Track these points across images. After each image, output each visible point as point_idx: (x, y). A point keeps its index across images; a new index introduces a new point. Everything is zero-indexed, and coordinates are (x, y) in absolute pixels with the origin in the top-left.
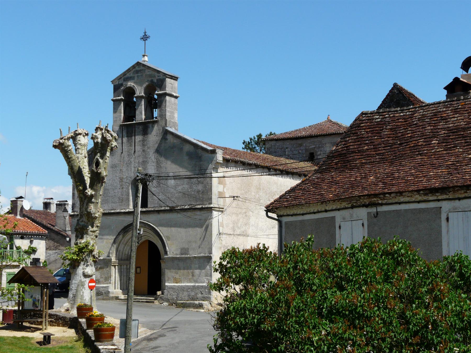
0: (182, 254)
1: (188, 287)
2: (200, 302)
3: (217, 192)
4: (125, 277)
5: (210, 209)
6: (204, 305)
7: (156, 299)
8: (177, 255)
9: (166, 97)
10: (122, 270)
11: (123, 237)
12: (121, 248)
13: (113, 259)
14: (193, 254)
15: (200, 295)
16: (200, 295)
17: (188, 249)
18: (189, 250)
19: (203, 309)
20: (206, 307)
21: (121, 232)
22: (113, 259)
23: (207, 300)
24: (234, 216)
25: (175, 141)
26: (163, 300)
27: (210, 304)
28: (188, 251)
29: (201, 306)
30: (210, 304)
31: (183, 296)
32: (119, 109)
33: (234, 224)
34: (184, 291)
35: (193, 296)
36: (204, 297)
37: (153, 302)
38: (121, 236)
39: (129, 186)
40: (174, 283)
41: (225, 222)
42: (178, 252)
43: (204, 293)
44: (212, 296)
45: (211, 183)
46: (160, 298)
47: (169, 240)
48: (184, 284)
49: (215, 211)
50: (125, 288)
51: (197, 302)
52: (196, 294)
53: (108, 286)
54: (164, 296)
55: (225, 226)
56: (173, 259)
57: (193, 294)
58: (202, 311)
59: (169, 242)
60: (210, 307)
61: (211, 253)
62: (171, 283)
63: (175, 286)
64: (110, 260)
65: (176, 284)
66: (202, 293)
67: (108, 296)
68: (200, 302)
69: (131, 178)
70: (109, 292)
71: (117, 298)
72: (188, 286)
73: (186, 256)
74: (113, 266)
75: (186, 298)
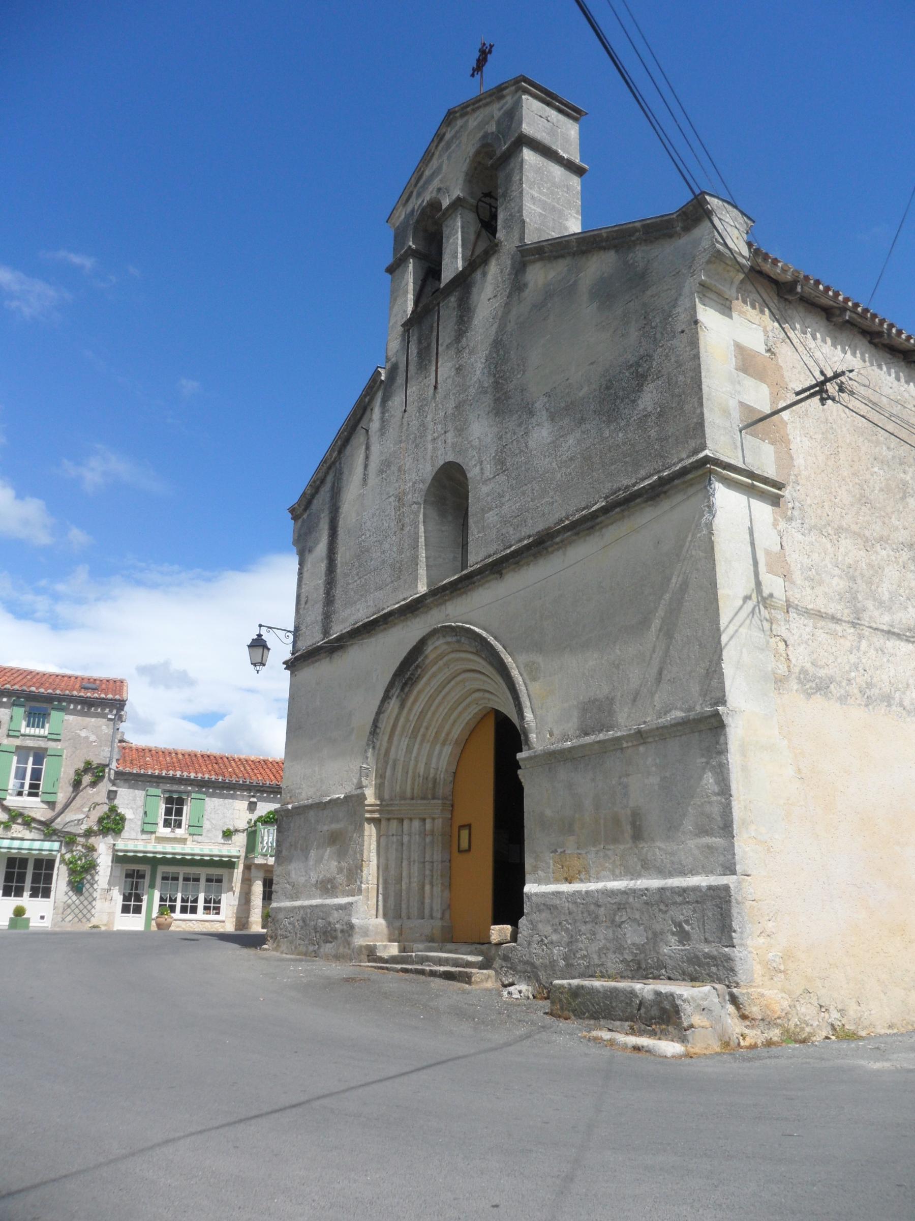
0: (587, 734)
1: (620, 902)
2: (665, 987)
3: (733, 404)
4: (415, 868)
5: (701, 472)
6: (687, 1008)
7: (486, 965)
8: (566, 738)
9: (521, 151)
10: (406, 839)
11: (402, 706)
12: (399, 750)
13: (371, 797)
14: (626, 721)
15: (671, 947)
16: (671, 947)
17: (611, 701)
18: (616, 707)
19: (682, 1033)
20: (697, 1020)
21: (391, 685)
22: (371, 797)
23: (714, 978)
24: (846, 543)
25: (552, 274)
26: (513, 968)
27: (734, 1000)
28: (611, 713)
29: (665, 1017)
30: (734, 1000)
31: (594, 947)
32: (403, 284)
33: (853, 579)
34: (596, 920)
35: (642, 948)
36: (694, 959)
37: (466, 978)
38: (393, 704)
39: (416, 514)
40: (557, 881)
41: (795, 558)
42: (572, 725)
43: (695, 934)
44: (736, 953)
45: (697, 357)
46: (506, 958)
47: (534, 679)
48: (600, 885)
49: (730, 483)
50: (395, 912)
51: (645, 989)
52: (656, 937)
53: (351, 904)
54: (520, 951)
55: (798, 577)
56: (555, 758)
57: (633, 936)
58: (670, 1047)
59: (535, 687)
60: (734, 1026)
61: (722, 701)
62: (548, 882)
63: (557, 894)
64: (363, 797)
65: (565, 888)
66: (684, 937)
67: (349, 944)
68: (665, 987)
69: (423, 481)
70: (352, 927)
71: (371, 953)
72: (612, 893)
73: (601, 737)
74: (370, 820)
75: (612, 962)
